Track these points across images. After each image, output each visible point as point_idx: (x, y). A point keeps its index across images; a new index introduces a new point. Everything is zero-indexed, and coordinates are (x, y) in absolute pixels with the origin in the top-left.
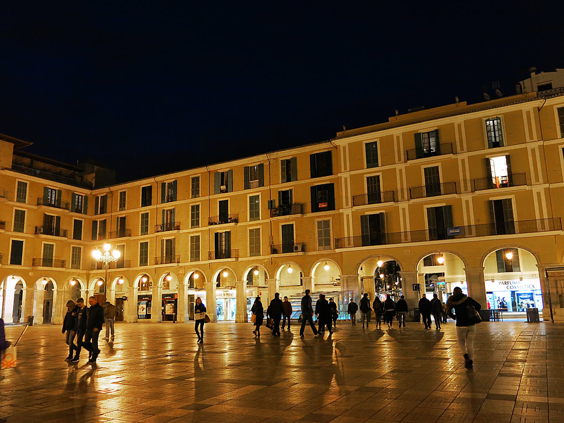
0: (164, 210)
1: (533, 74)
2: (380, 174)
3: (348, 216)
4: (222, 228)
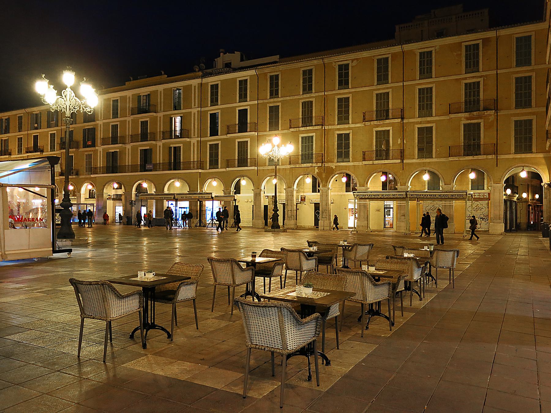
0: (2, 140)
1: (221, 54)
2: (248, 108)
3: (160, 146)
4: (113, 148)
